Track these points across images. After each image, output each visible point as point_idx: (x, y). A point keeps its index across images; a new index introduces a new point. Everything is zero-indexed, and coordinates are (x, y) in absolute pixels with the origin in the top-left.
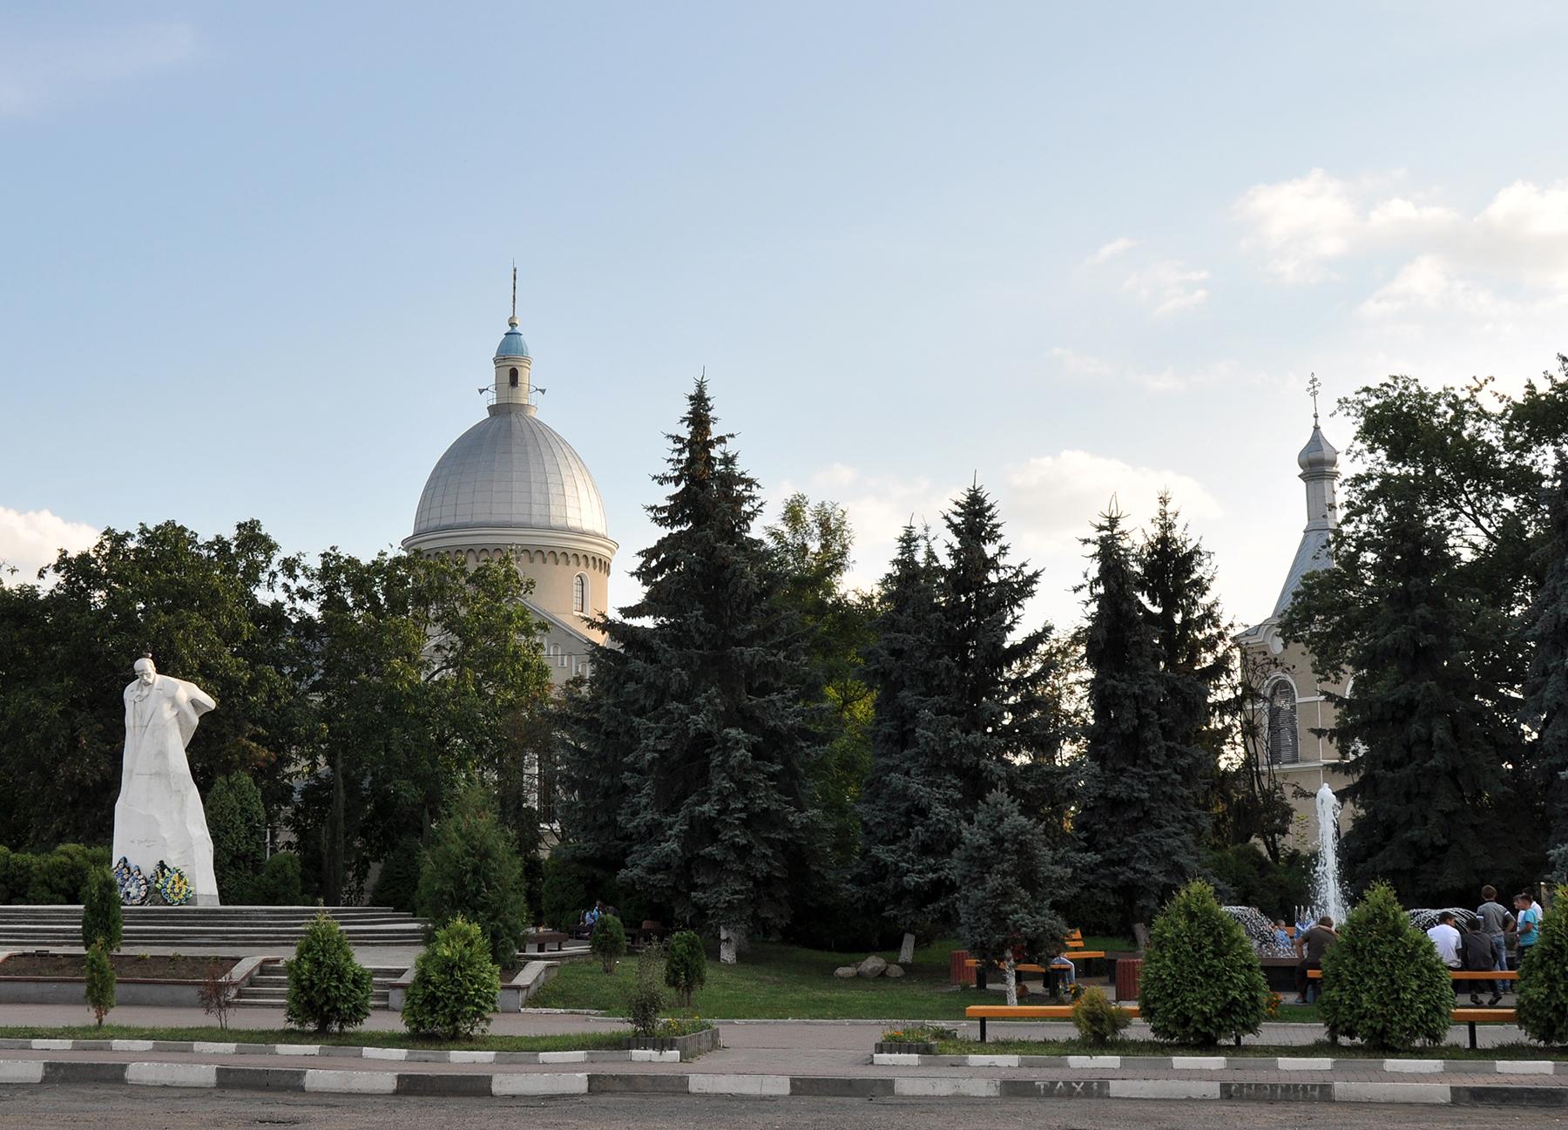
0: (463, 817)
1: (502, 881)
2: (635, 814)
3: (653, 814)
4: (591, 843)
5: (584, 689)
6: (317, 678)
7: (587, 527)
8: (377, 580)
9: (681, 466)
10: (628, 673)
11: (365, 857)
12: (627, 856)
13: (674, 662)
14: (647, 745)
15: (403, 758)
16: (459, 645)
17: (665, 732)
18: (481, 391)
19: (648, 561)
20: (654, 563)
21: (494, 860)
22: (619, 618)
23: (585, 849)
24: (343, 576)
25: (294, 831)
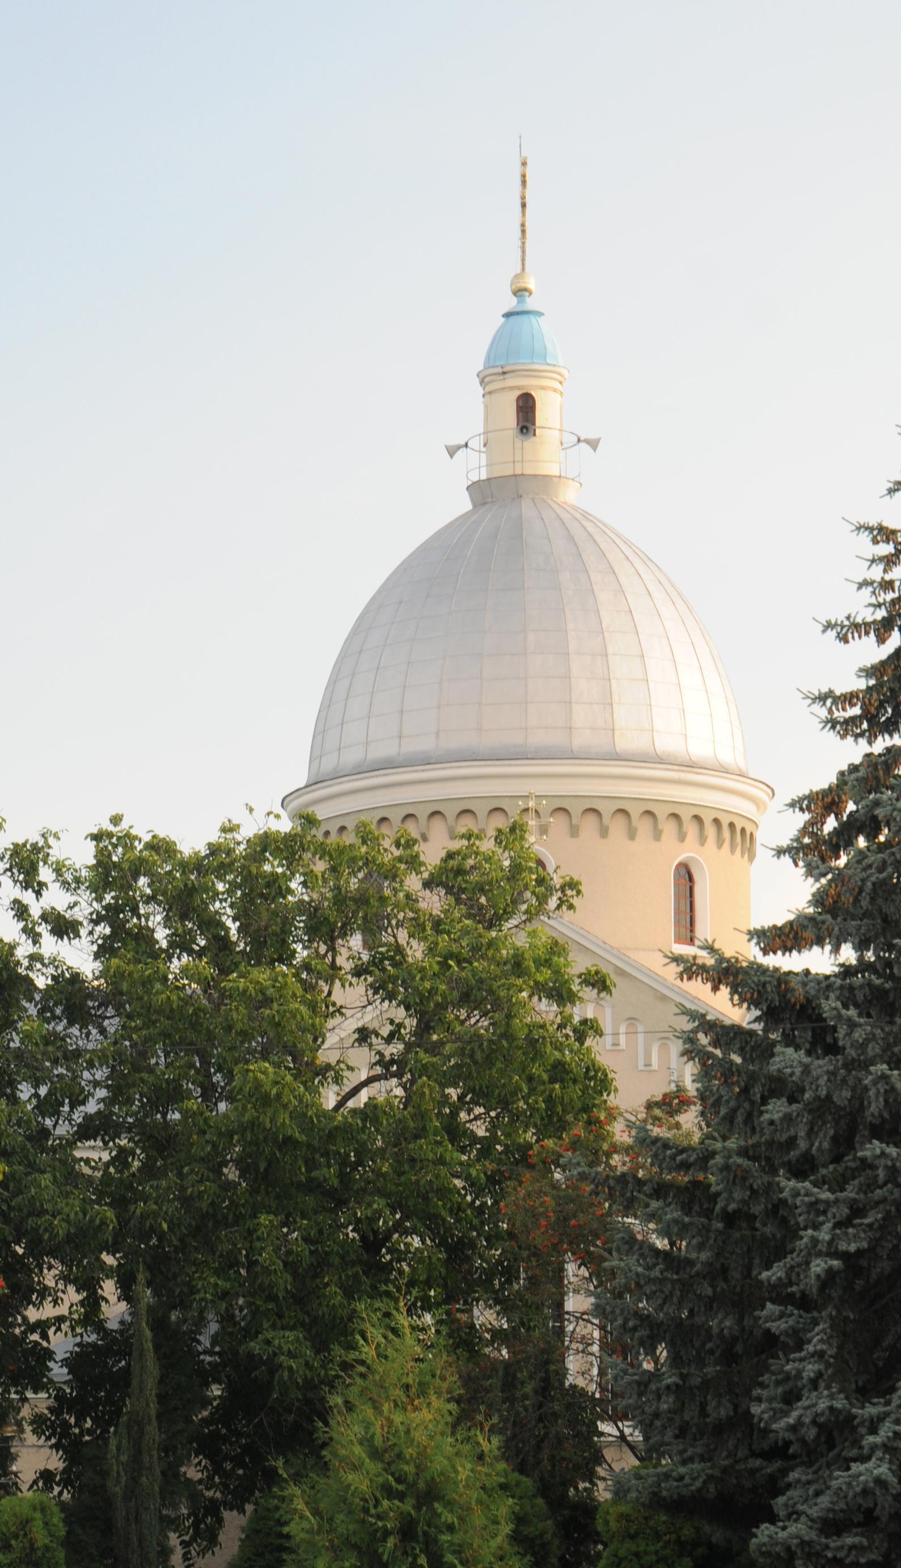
0: (377, 1408)
1: (468, 1553)
2: (791, 1398)
3: (831, 1397)
4: (696, 1466)
5: (690, 1120)
6: (92, 1107)
7: (699, 749)
8: (221, 887)
9: (890, 596)
10: (771, 1078)
11: (212, 1500)
12: (781, 1492)
13: (874, 1049)
14: (815, 1241)
15: (284, 1282)
16: (411, 1023)
17: (857, 1211)
18: (452, 451)
19: (818, 821)
20: (831, 824)
21: (449, 1504)
22: (752, 953)
23: (681, 1478)
24: (143, 881)
25: (57, 1447)
